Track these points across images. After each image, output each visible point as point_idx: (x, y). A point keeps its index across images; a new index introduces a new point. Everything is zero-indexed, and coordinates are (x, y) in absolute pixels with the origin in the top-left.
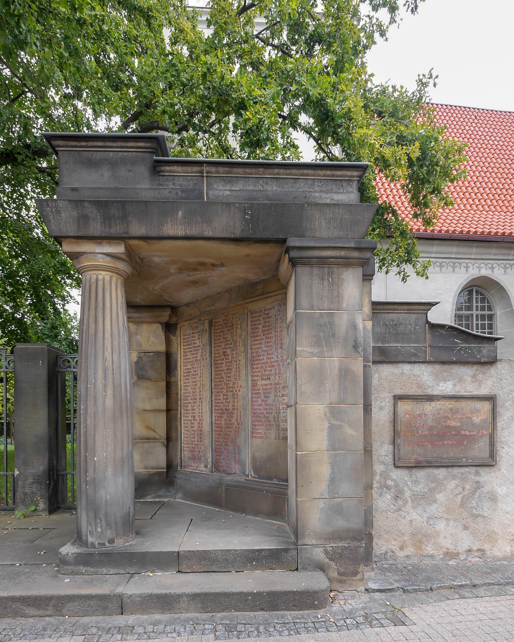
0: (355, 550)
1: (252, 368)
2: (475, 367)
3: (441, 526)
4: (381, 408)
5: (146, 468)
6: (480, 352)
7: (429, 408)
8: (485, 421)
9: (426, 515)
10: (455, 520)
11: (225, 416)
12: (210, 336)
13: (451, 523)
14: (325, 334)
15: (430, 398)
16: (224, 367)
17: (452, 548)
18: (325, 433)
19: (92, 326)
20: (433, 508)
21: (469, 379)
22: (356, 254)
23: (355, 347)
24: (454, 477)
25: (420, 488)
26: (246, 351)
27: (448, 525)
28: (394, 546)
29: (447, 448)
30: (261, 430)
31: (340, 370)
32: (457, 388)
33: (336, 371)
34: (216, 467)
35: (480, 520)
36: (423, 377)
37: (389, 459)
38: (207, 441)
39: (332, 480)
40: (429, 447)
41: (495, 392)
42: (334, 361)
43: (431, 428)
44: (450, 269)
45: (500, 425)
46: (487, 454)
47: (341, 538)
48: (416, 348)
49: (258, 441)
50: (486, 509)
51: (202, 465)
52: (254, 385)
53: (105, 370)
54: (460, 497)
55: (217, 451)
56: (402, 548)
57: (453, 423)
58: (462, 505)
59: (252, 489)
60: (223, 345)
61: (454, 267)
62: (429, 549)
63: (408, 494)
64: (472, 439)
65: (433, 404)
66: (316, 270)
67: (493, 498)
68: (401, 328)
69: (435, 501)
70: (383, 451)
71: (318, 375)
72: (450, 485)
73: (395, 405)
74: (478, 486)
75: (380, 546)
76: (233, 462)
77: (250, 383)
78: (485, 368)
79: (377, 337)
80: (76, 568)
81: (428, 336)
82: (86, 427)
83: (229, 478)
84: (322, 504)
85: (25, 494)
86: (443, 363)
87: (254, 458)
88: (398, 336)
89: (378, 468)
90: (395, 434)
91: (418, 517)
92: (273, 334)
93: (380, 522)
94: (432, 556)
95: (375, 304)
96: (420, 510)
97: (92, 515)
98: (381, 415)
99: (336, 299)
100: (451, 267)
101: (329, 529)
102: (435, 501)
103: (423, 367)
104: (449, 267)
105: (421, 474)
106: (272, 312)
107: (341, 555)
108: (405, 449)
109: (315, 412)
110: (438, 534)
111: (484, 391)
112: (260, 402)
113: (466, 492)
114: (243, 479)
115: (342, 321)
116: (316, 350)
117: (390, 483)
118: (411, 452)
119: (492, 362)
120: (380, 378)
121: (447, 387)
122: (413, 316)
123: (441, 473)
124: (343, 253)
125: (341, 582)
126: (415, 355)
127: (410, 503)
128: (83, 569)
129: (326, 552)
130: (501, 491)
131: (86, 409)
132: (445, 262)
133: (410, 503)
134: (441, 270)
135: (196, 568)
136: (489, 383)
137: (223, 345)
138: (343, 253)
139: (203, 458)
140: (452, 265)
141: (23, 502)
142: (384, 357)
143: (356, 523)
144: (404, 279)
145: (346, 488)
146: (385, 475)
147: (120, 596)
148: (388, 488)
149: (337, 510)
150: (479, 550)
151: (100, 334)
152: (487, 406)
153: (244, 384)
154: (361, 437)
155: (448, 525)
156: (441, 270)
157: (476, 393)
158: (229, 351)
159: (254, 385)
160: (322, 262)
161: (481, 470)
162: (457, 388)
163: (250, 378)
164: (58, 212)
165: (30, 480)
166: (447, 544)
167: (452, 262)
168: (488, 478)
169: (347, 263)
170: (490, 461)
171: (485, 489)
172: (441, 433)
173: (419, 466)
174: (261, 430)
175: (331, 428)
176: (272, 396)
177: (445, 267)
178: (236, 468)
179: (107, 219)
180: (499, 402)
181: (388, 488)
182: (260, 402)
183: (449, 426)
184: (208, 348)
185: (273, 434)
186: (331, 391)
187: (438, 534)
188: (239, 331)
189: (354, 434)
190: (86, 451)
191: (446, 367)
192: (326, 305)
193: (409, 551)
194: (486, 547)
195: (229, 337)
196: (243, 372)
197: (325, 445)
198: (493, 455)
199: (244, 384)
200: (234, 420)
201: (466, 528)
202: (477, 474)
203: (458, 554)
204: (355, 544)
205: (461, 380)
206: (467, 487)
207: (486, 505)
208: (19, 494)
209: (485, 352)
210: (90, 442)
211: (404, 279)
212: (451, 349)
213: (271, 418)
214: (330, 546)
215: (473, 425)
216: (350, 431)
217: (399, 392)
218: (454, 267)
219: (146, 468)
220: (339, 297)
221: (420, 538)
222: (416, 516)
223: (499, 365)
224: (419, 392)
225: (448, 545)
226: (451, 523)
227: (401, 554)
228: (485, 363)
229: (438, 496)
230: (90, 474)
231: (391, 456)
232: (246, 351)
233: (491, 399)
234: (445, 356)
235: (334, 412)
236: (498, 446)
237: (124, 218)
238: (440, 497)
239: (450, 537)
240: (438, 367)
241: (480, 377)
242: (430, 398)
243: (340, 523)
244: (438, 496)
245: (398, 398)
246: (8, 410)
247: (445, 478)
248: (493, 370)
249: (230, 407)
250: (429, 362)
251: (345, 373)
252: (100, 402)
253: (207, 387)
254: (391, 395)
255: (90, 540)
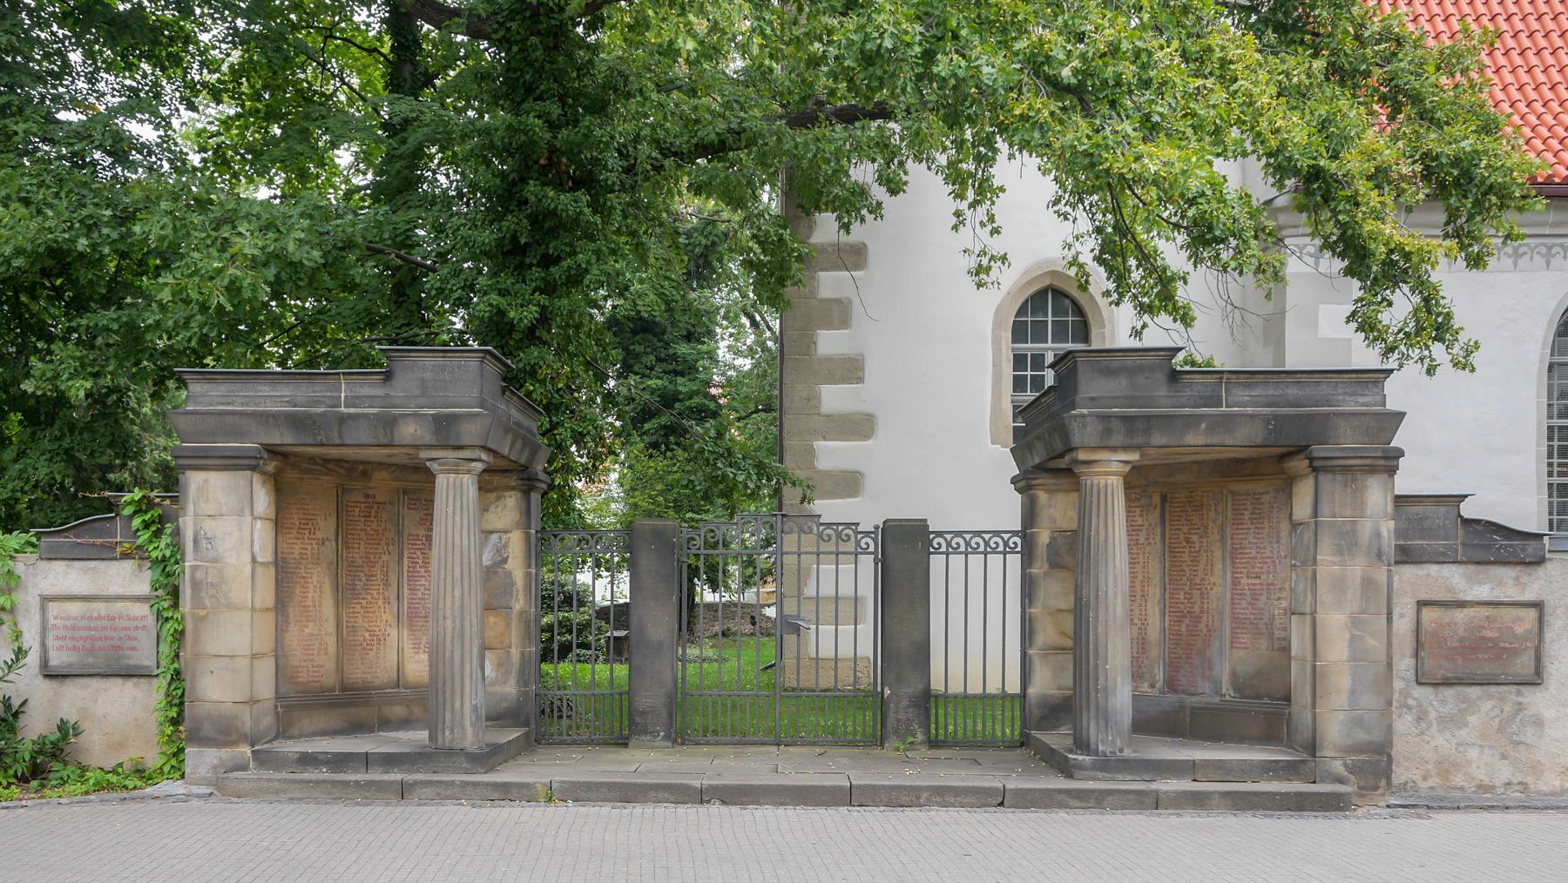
0: (1374, 768)
1: (1233, 563)
2: (1519, 568)
3: (1473, 753)
4: (1402, 616)
5: (1060, 688)
6: (1523, 550)
7: (1460, 615)
8: (1529, 632)
9: (1455, 741)
10: (1491, 747)
11: (1187, 621)
12: (1163, 515)
13: (1486, 751)
14: (1348, 541)
15: (1462, 604)
16: (1186, 557)
17: (1486, 780)
18: (1346, 644)
19: (1102, 534)
20: (1464, 732)
21: (1511, 582)
22: (1382, 462)
23: (1379, 555)
24: (1490, 697)
25: (1446, 709)
26: (1222, 539)
27: (1482, 752)
28: (1416, 775)
29: (1486, 663)
30: (1245, 639)
31: (1363, 580)
32: (1495, 593)
33: (1358, 580)
34: (1171, 685)
35: (1521, 747)
36: (1454, 579)
37: (1411, 674)
38: (1154, 653)
39: (1353, 692)
40: (1460, 661)
41: (1544, 597)
42: (1356, 569)
43: (1462, 639)
44: (1539, 260)
45: (1548, 636)
46: (1532, 670)
47: (1361, 752)
48: (1445, 546)
49: (1241, 653)
50: (1530, 735)
51: (1146, 685)
52: (1236, 583)
53: (1115, 578)
54: (1497, 721)
55: (1173, 666)
56: (1425, 778)
57: (1489, 634)
58: (1500, 730)
59: (1233, 711)
60: (1185, 529)
61: (1548, 257)
62: (1459, 780)
63: (1433, 715)
64: (1514, 653)
65: (1466, 611)
66: (1339, 477)
67: (1539, 723)
68: (1428, 523)
69: (1467, 725)
70: (1404, 665)
71: (1339, 584)
72: (1486, 705)
73: (1418, 612)
74: (1520, 707)
75: (1400, 775)
76: (1199, 679)
77: (1229, 580)
78: (1528, 570)
79: (1399, 533)
80: (1093, 774)
81: (1460, 532)
82: (1096, 635)
83: (1194, 699)
84: (1341, 716)
85: (898, 721)
86: (1478, 563)
87: (1234, 674)
88: (1425, 532)
89: (1398, 685)
90: (1418, 645)
91: (1439, 735)
92: (1266, 524)
93: (1399, 749)
94: (1461, 789)
95: (1397, 497)
96: (1448, 734)
97: (1102, 723)
98: (1403, 624)
99: (1359, 507)
100: (1543, 256)
101: (1350, 742)
102: (1467, 725)
103: (1454, 567)
104: (1537, 257)
105: (1449, 692)
106: (1265, 498)
107: (1361, 769)
108: (1430, 664)
109: (1335, 621)
110: (1469, 762)
111: (1529, 596)
112: (1244, 604)
113: (1505, 715)
114: (1217, 700)
115: (1365, 529)
116: (1337, 559)
117: (1411, 702)
118: (1436, 666)
119: (1540, 561)
120: (1401, 581)
121: (1482, 592)
122: (1443, 509)
123: (1474, 692)
124: (1368, 462)
125: (1361, 796)
126: (1443, 554)
127: (1435, 726)
128: (1100, 775)
129: (1345, 765)
130: (1549, 714)
131: (1097, 617)
132: (1527, 245)
133: (1435, 726)
134: (1515, 263)
135: (1211, 777)
136: (1536, 586)
137: (1185, 529)
138: (1368, 462)
139: (1147, 676)
140: (1544, 250)
141: (896, 732)
142: (1406, 556)
143: (1376, 737)
144: (1431, 371)
145: (1368, 700)
146: (1405, 693)
147: (1156, 792)
148: (1409, 708)
149: (1358, 722)
150: (1520, 783)
151: (1110, 541)
152: (1532, 614)
153: (1219, 581)
154: (1384, 648)
155: (1482, 752)
156: (1515, 263)
157: (1518, 598)
158: (1195, 538)
159: (1236, 583)
160: (1346, 469)
161: (1523, 689)
162: (1495, 593)
163: (1229, 575)
164: (1084, 426)
165: (905, 702)
166: (1481, 775)
167: (1545, 245)
168: (1530, 696)
169: (1372, 470)
170: (1536, 679)
171: (1530, 712)
172: (1474, 645)
173: (1446, 683)
174: (1245, 639)
175: (1353, 639)
176: (1263, 598)
177: (1526, 258)
178: (1206, 687)
179: (1130, 432)
180: (1548, 610)
181: (1409, 708)
182: (1244, 604)
183: (1484, 638)
184: (1158, 530)
185: (1264, 644)
186: (1353, 601)
187: (1469, 762)
188: (1212, 514)
189: (1375, 645)
190: (1096, 658)
191: (1481, 568)
192: (1349, 512)
193: (1434, 781)
194: (1529, 779)
195: (1196, 519)
196: (1219, 566)
197: (1345, 655)
198: (1539, 671)
199: (1219, 581)
200: (1202, 626)
201: (1504, 757)
202: (1519, 693)
203: (1494, 787)
204: (1377, 757)
205: (1500, 583)
206: (1507, 709)
207: (1530, 730)
208: (891, 721)
209: (1530, 550)
210: (1101, 649)
211: (1431, 371)
212: (1488, 547)
213: (1261, 625)
214: (1350, 759)
215: (1515, 636)
216: (1371, 642)
217: (1424, 597)
218: (1548, 257)
219: (1060, 688)
220: (1363, 504)
221: (1447, 767)
222: (1442, 742)
223: (1549, 565)
224: (1449, 597)
225: (1482, 777)
226: (1486, 751)
227: (1423, 785)
228: (1530, 563)
229: (1469, 719)
230: (1101, 682)
231: (1413, 671)
232: (1222, 539)
233: (1538, 605)
234: (1480, 555)
235: (1356, 622)
236: (1546, 661)
237: (1147, 431)
238: (1473, 720)
239: (1484, 765)
240: (1472, 568)
241: (1525, 579)
242: (1462, 604)
243: (1361, 736)
244: (1469, 719)
245: (1421, 604)
246: (393, 600)
247: (1479, 698)
248: (1540, 571)
249: (1197, 609)
250: (1461, 563)
251: (1368, 583)
252: (1111, 610)
253: (1157, 580)
254: (1414, 601)
255: (1101, 748)
